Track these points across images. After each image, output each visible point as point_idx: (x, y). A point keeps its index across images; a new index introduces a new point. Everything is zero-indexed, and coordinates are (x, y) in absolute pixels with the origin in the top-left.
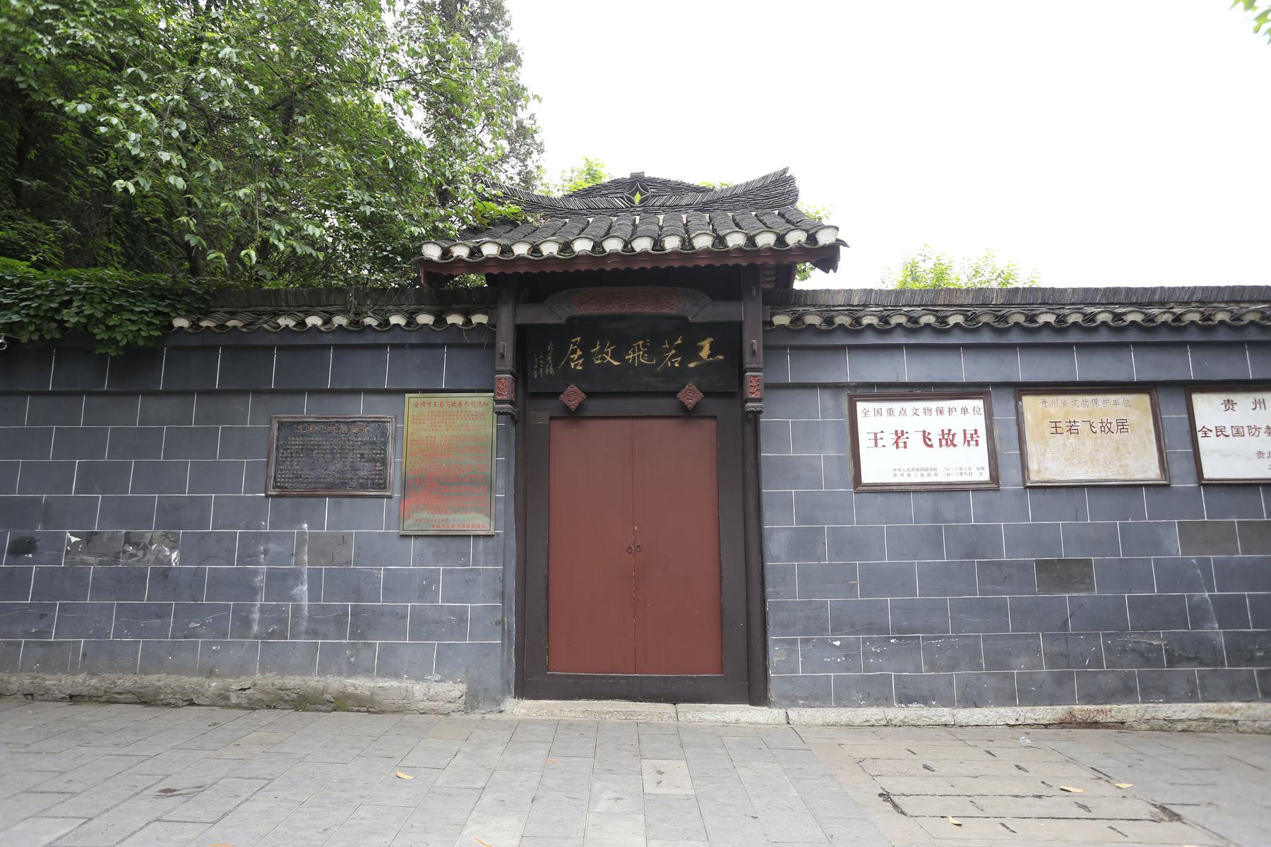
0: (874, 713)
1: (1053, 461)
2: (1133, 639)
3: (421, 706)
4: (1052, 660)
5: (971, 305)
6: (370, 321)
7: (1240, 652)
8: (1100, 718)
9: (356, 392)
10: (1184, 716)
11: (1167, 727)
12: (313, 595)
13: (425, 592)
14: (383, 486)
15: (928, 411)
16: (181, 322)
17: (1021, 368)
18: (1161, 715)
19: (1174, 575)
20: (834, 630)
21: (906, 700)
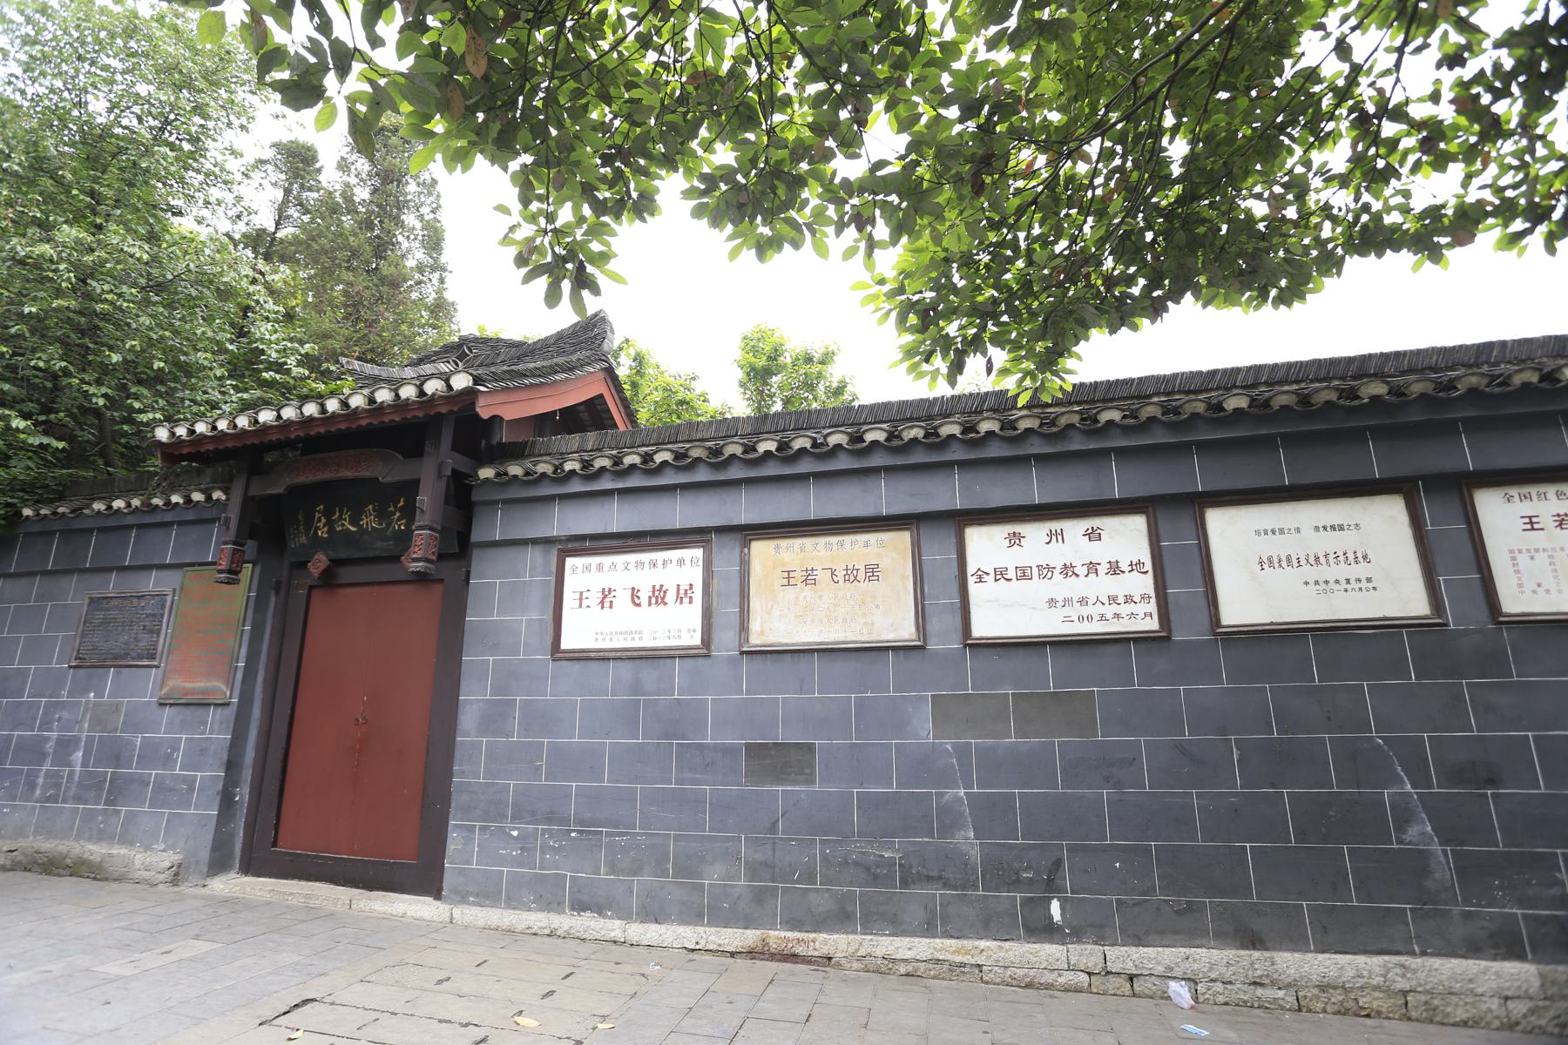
0: (538, 920)
1: (781, 618)
2: (858, 848)
3: (137, 875)
4: (753, 871)
5: (714, 439)
6: (157, 501)
7: (1000, 873)
8: (800, 950)
9: (149, 567)
10: (909, 955)
11: (885, 968)
12: (85, 764)
13: (168, 761)
14: (153, 657)
15: (640, 564)
16: (27, 512)
17: (745, 508)
18: (880, 952)
19: (922, 766)
20: (516, 818)
21: (580, 907)
